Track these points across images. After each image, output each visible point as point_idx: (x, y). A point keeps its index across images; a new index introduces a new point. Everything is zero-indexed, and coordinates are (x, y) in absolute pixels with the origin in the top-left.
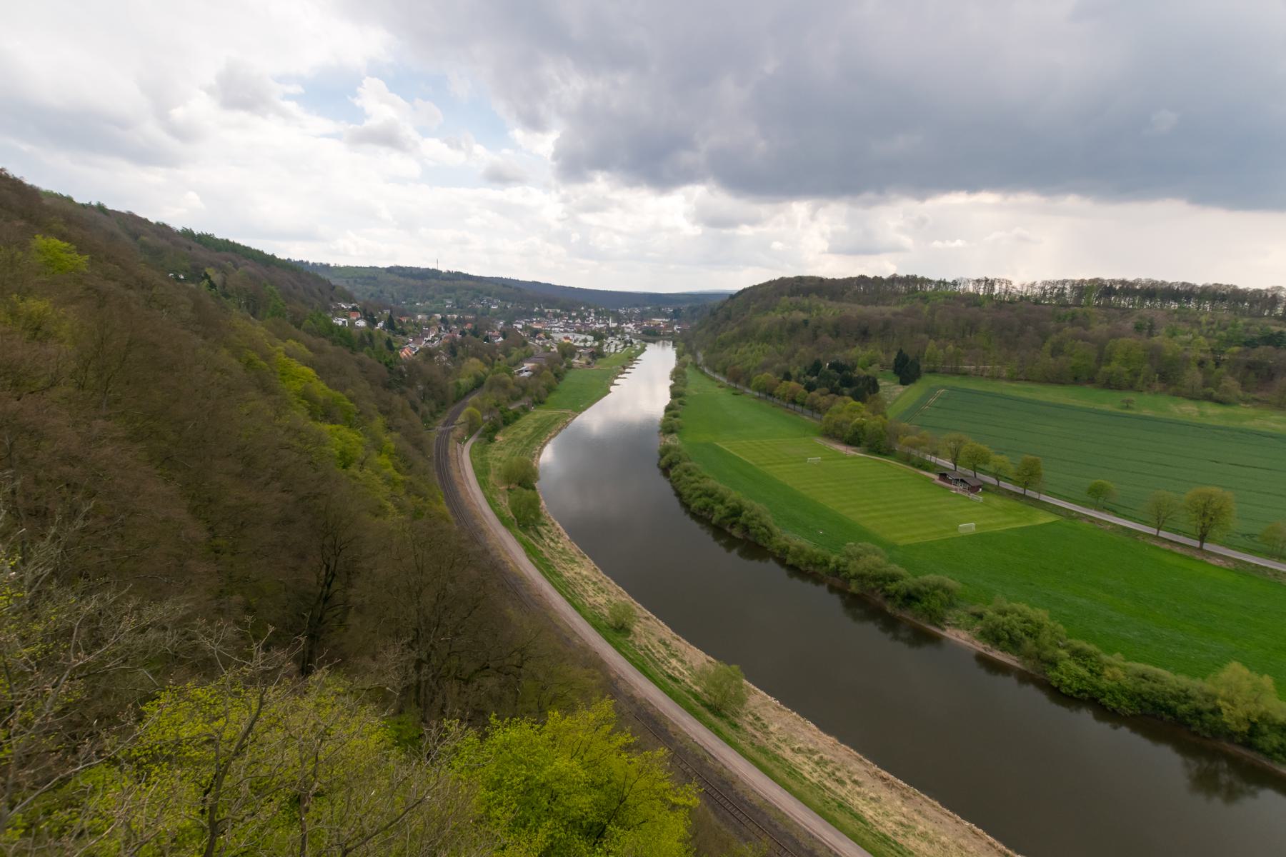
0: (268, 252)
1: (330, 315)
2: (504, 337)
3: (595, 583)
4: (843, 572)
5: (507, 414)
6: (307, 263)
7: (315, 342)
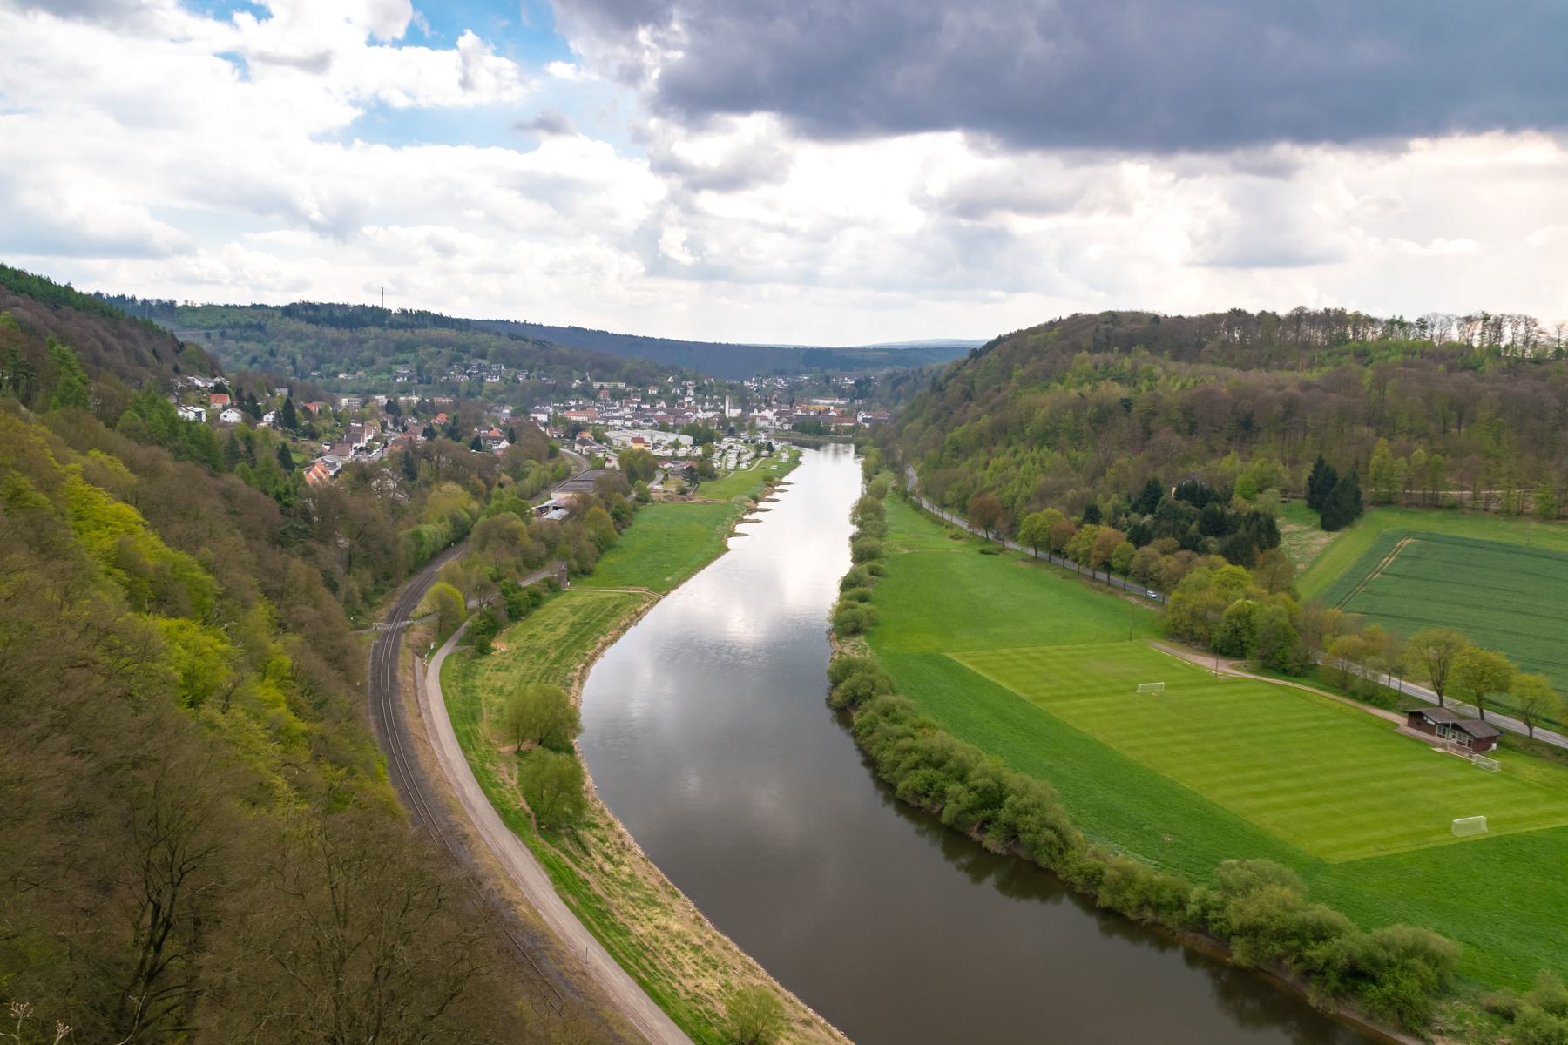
0: (59, 280)
1: (172, 401)
2: (512, 440)
3: (696, 949)
4: (1215, 921)
5: (517, 596)
6: (133, 299)
7: (143, 453)
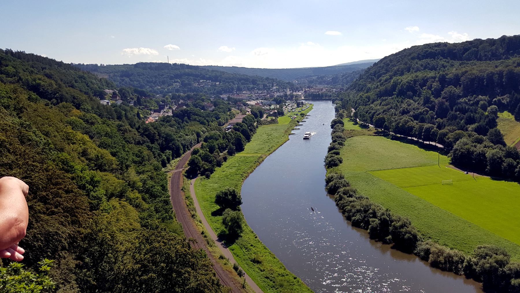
6: (83, 64)
